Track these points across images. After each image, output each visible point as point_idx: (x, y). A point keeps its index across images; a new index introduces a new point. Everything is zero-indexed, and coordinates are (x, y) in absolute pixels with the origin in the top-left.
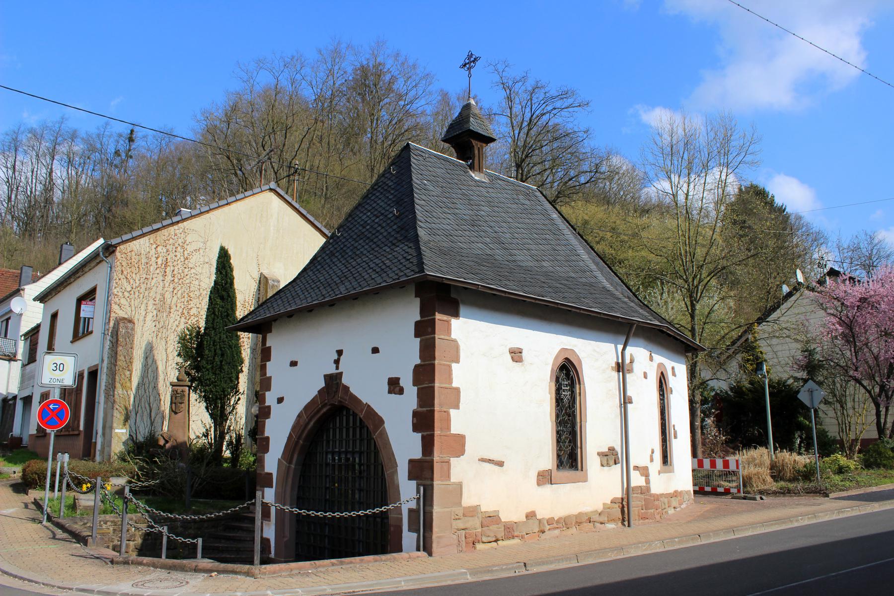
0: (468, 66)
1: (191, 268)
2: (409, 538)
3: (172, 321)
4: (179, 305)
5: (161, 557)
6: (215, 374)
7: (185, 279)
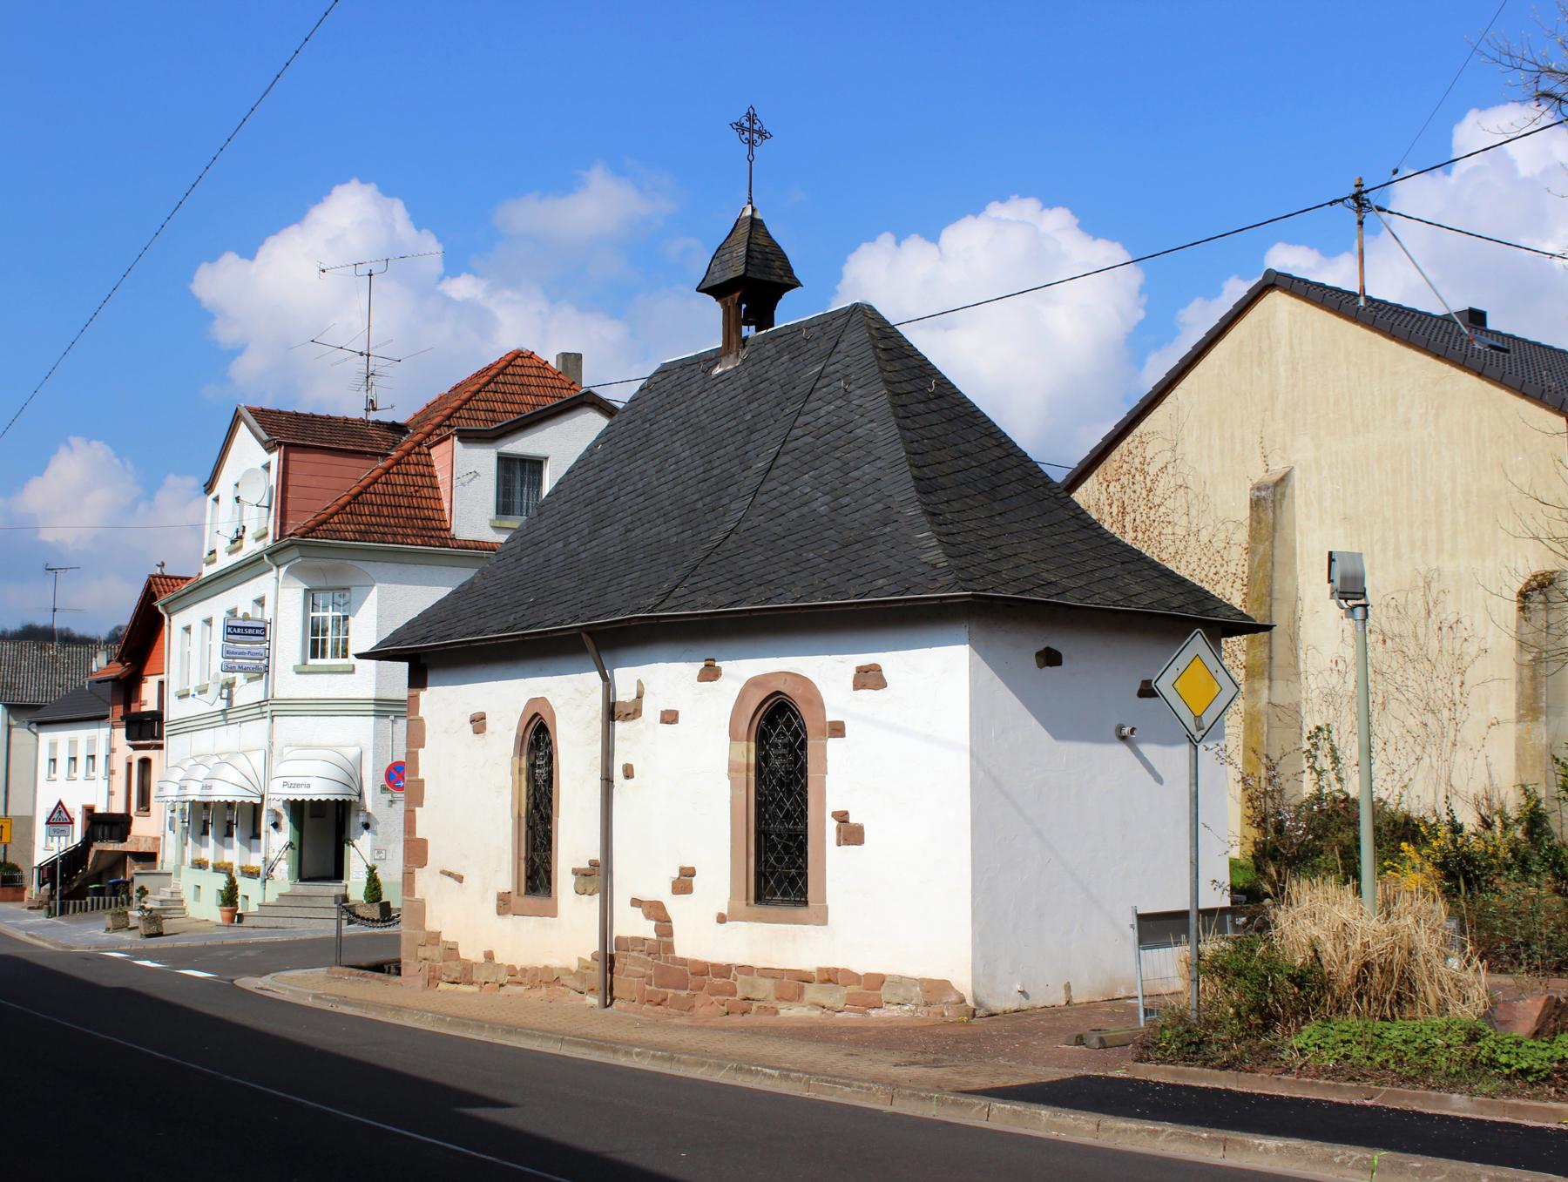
1: (1159, 506)
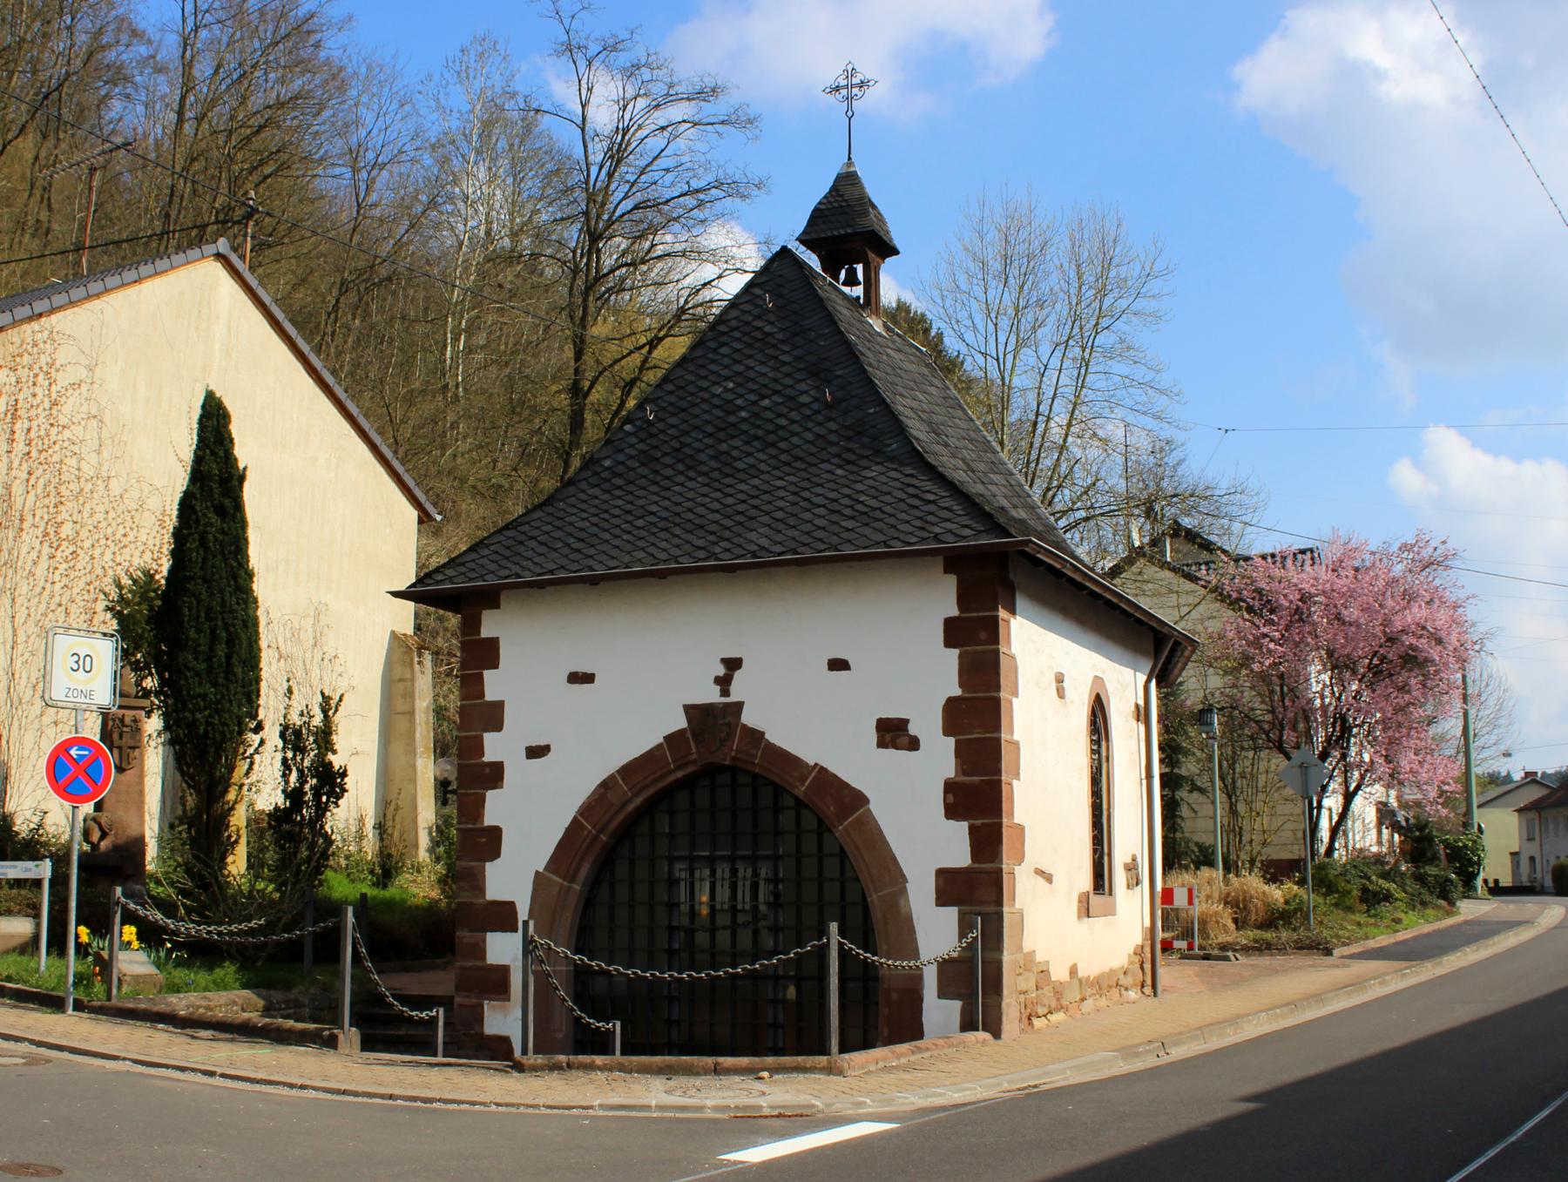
2: (939, 1011)
3: (24, 550)
4: (39, 513)
5: (614, 1054)
6: (215, 684)
7: (50, 451)
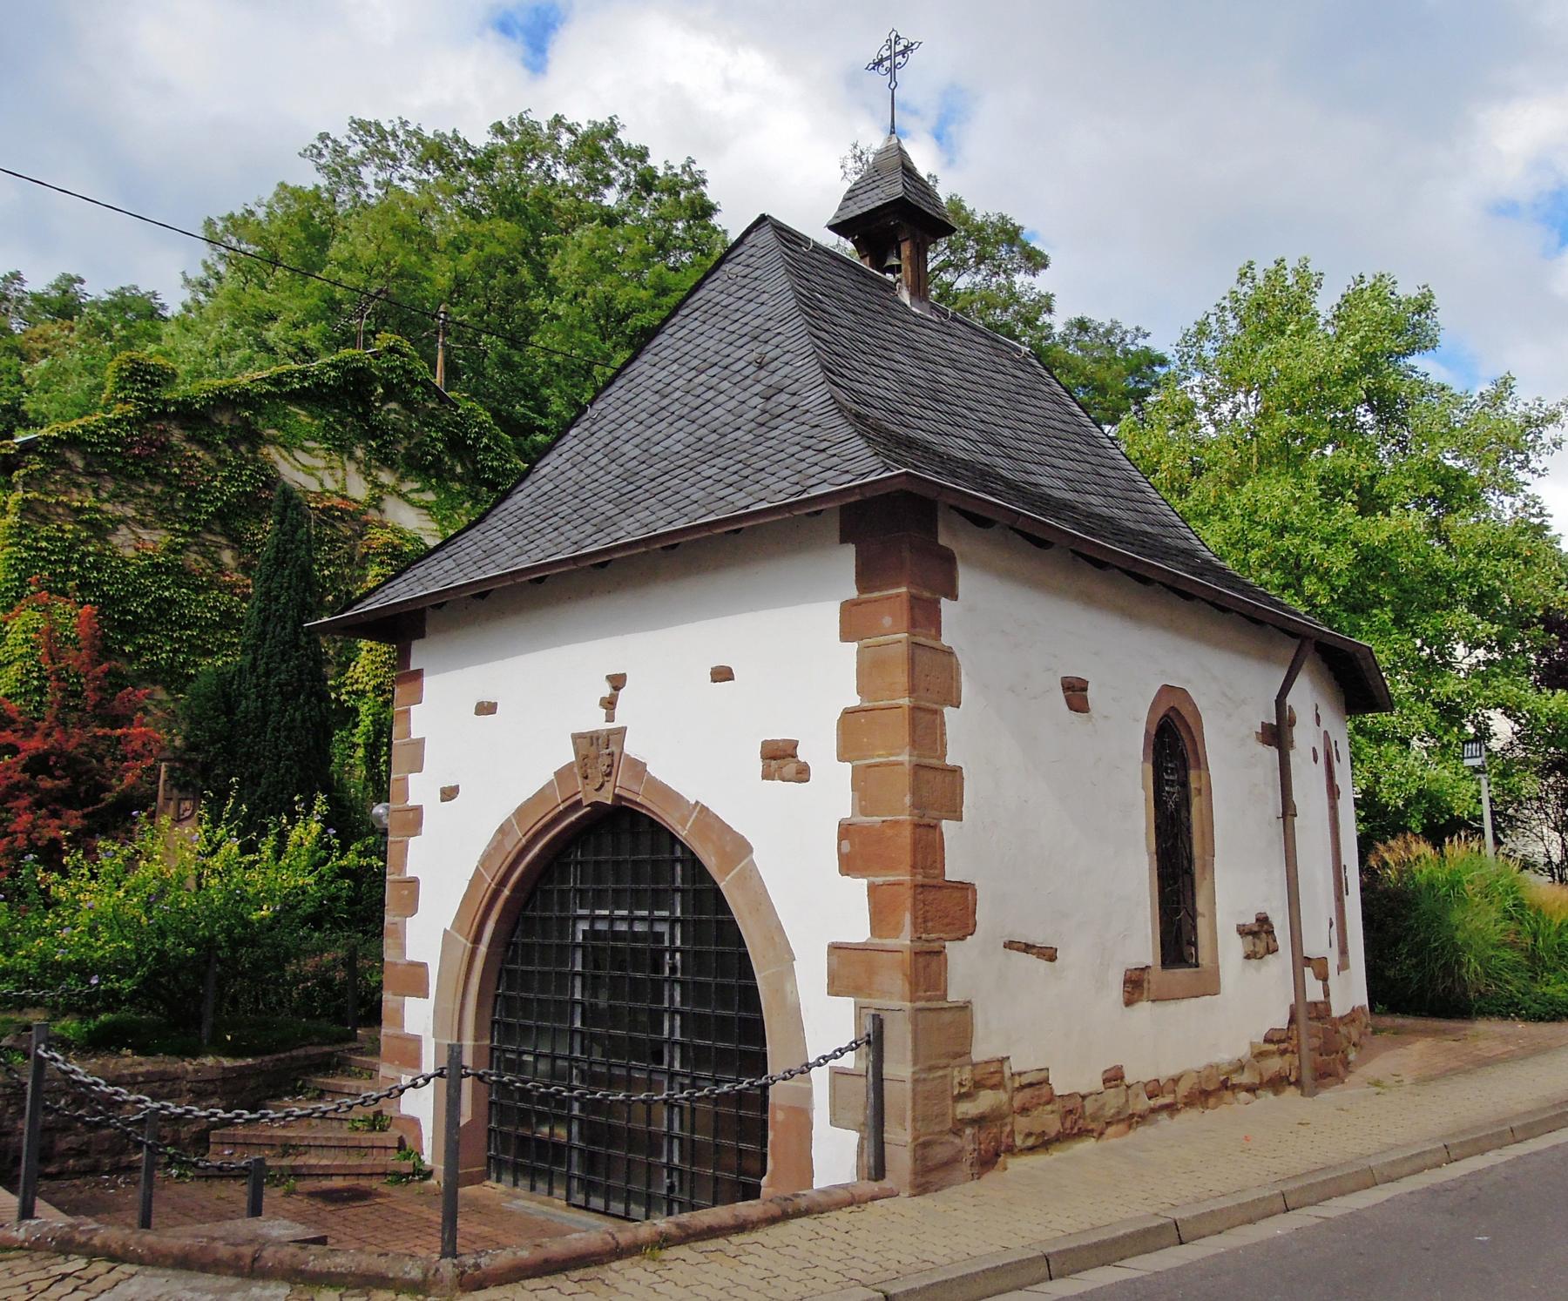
0: (887, 64)
